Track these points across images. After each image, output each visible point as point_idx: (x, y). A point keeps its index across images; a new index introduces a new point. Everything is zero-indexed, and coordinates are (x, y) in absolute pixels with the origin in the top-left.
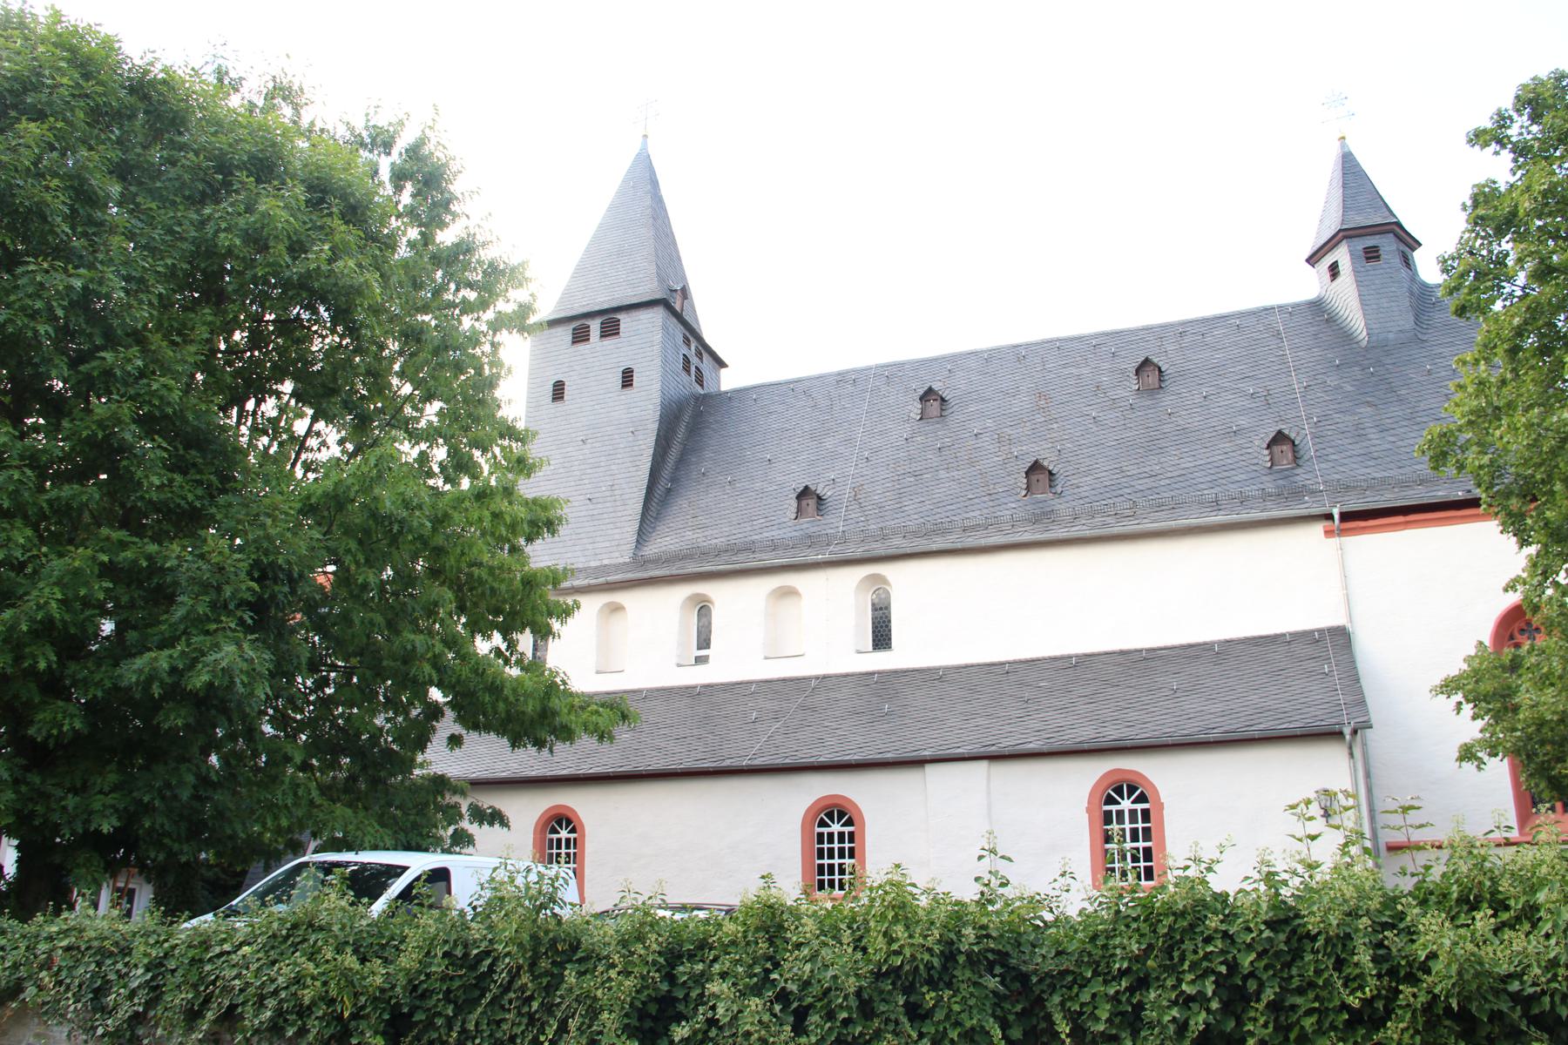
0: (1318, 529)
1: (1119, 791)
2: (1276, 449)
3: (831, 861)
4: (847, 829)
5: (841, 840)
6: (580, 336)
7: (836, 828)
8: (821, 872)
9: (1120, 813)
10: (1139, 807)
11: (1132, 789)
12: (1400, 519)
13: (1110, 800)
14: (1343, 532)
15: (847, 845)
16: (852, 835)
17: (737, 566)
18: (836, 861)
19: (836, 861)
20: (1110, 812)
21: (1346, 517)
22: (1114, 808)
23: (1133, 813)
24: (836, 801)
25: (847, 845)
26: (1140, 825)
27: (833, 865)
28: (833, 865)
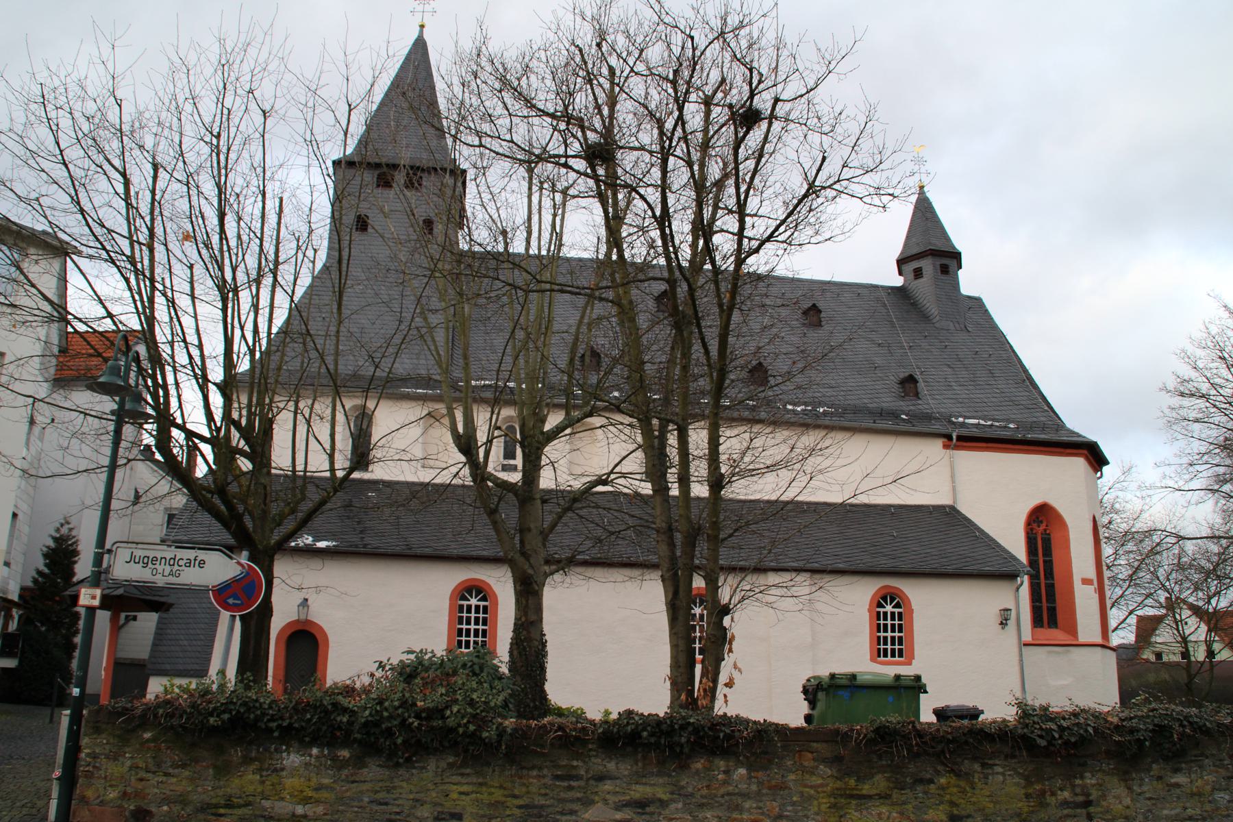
0: (939, 443)
1: (884, 599)
2: (907, 385)
3: (885, 634)
4: (482, 603)
5: (477, 611)
6: (384, 182)
7: (474, 602)
8: (460, 634)
9: (885, 614)
10: (896, 610)
11: (892, 600)
12: (1000, 445)
13: (880, 605)
14: (957, 448)
15: (481, 615)
16: (485, 609)
17: (1043, 437)
18: (889, 634)
19: (889, 634)
20: (463, 606)
21: (960, 438)
22: (882, 610)
23: (893, 614)
24: (476, 584)
25: (481, 615)
26: (897, 622)
27: (470, 630)
28: (470, 630)
